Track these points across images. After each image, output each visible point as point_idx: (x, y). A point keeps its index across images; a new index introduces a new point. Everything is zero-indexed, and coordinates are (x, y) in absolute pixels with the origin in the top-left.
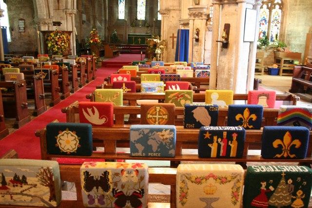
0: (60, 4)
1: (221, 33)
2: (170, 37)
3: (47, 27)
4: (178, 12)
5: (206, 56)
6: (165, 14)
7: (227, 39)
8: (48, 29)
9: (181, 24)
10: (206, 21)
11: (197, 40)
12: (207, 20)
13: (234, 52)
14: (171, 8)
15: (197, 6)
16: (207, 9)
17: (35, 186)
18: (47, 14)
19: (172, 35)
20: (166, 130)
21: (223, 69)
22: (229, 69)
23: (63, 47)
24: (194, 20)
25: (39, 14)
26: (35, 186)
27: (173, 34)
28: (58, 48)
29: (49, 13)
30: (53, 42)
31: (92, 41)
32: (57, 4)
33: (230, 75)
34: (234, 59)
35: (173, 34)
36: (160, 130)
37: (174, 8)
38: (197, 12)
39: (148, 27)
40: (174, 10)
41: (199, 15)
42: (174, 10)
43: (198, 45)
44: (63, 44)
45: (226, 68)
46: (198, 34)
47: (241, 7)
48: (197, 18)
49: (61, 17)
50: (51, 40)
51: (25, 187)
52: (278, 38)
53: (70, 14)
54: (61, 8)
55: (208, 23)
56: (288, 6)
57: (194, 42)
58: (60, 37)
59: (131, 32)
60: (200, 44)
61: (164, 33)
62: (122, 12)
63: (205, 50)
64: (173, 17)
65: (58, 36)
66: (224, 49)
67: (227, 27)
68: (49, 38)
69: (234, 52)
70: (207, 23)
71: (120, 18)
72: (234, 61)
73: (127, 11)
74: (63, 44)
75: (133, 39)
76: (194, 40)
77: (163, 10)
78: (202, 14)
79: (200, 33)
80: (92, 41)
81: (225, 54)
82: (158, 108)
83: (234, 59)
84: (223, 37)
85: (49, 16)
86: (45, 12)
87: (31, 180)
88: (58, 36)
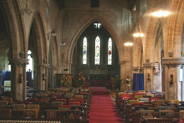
0: (64, 59)
1: (170, 79)
2: (126, 77)
3: (56, 72)
4: (130, 63)
5: (154, 87)
6: (123, 64)
7: (172, 80)
8: (57, 72)
9: (133, 70)
10: (152, 70)
11: (149, 79)
12: (153, 70)
13: (175, 85)
14: (127, 61)
15: (148, 63)
16: (153, 64)
17: (150, 116)
18: (56, 64)
19: (127, 76)
20: (169, 108)
21: (171, 93)
22: (174, 93)
23: (70, 83)
24: (146, 69)
25: (53, 64)
26: (150, 116)
27: (128, 75)
28: (67, 83)
29: (58, 64)
30: (64, 80)
31: (80, 79)
32: (62, 58)
33: (174, 95)
34: (175, 88)
35: (128, 75)
36: (167, 108)
37: (128, 61)
38: (148, 66)
39: (102, 69)
40: (128, 62)
41: (149, 67)
42: (128, 62)
43: (149, 82)
44: (69, 81)
45: (172, 92)
46: (149, 77)
47: (177, 69)
48: (148, 69)
49: (64, 66)
50: (63, 79)
51: (148, 116)
52: (49, 38)
53: (69, 64)
54: (64, 61)
55: (154, 71)
56: (164, 38)
57: (147, 80)
58: (68, 78)
59: (92, 72)
60: (150, 81)
61: (123, 75)
62: (85, 60)
63: (153, 84)
64: (127, 66)
65: (67, 77)
66: (171, 85)
67: (172, 76)
68: (62, 78)
69: (175, 85)
70: (153, 71)
71: (83, 64)
72: (175, 89)
73: (88, 59)
74: (69, 81)
75: (93, 77)
76: (147, 79)
77: (122, 62)
78: (150, 66)
79: (150, 76)
80: (80, 79)
81: (171, 87)
82: (158, 105)
83: (175, 88)
84: (170, 80)
85: (58, 65)
86: (56, 62)
87: (149, 114)
88: (67, 77)
